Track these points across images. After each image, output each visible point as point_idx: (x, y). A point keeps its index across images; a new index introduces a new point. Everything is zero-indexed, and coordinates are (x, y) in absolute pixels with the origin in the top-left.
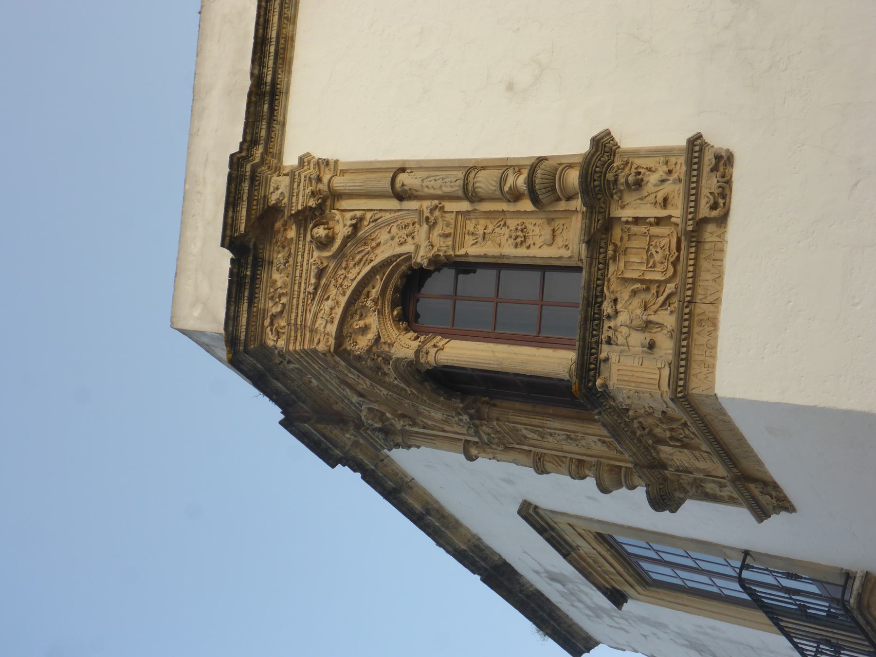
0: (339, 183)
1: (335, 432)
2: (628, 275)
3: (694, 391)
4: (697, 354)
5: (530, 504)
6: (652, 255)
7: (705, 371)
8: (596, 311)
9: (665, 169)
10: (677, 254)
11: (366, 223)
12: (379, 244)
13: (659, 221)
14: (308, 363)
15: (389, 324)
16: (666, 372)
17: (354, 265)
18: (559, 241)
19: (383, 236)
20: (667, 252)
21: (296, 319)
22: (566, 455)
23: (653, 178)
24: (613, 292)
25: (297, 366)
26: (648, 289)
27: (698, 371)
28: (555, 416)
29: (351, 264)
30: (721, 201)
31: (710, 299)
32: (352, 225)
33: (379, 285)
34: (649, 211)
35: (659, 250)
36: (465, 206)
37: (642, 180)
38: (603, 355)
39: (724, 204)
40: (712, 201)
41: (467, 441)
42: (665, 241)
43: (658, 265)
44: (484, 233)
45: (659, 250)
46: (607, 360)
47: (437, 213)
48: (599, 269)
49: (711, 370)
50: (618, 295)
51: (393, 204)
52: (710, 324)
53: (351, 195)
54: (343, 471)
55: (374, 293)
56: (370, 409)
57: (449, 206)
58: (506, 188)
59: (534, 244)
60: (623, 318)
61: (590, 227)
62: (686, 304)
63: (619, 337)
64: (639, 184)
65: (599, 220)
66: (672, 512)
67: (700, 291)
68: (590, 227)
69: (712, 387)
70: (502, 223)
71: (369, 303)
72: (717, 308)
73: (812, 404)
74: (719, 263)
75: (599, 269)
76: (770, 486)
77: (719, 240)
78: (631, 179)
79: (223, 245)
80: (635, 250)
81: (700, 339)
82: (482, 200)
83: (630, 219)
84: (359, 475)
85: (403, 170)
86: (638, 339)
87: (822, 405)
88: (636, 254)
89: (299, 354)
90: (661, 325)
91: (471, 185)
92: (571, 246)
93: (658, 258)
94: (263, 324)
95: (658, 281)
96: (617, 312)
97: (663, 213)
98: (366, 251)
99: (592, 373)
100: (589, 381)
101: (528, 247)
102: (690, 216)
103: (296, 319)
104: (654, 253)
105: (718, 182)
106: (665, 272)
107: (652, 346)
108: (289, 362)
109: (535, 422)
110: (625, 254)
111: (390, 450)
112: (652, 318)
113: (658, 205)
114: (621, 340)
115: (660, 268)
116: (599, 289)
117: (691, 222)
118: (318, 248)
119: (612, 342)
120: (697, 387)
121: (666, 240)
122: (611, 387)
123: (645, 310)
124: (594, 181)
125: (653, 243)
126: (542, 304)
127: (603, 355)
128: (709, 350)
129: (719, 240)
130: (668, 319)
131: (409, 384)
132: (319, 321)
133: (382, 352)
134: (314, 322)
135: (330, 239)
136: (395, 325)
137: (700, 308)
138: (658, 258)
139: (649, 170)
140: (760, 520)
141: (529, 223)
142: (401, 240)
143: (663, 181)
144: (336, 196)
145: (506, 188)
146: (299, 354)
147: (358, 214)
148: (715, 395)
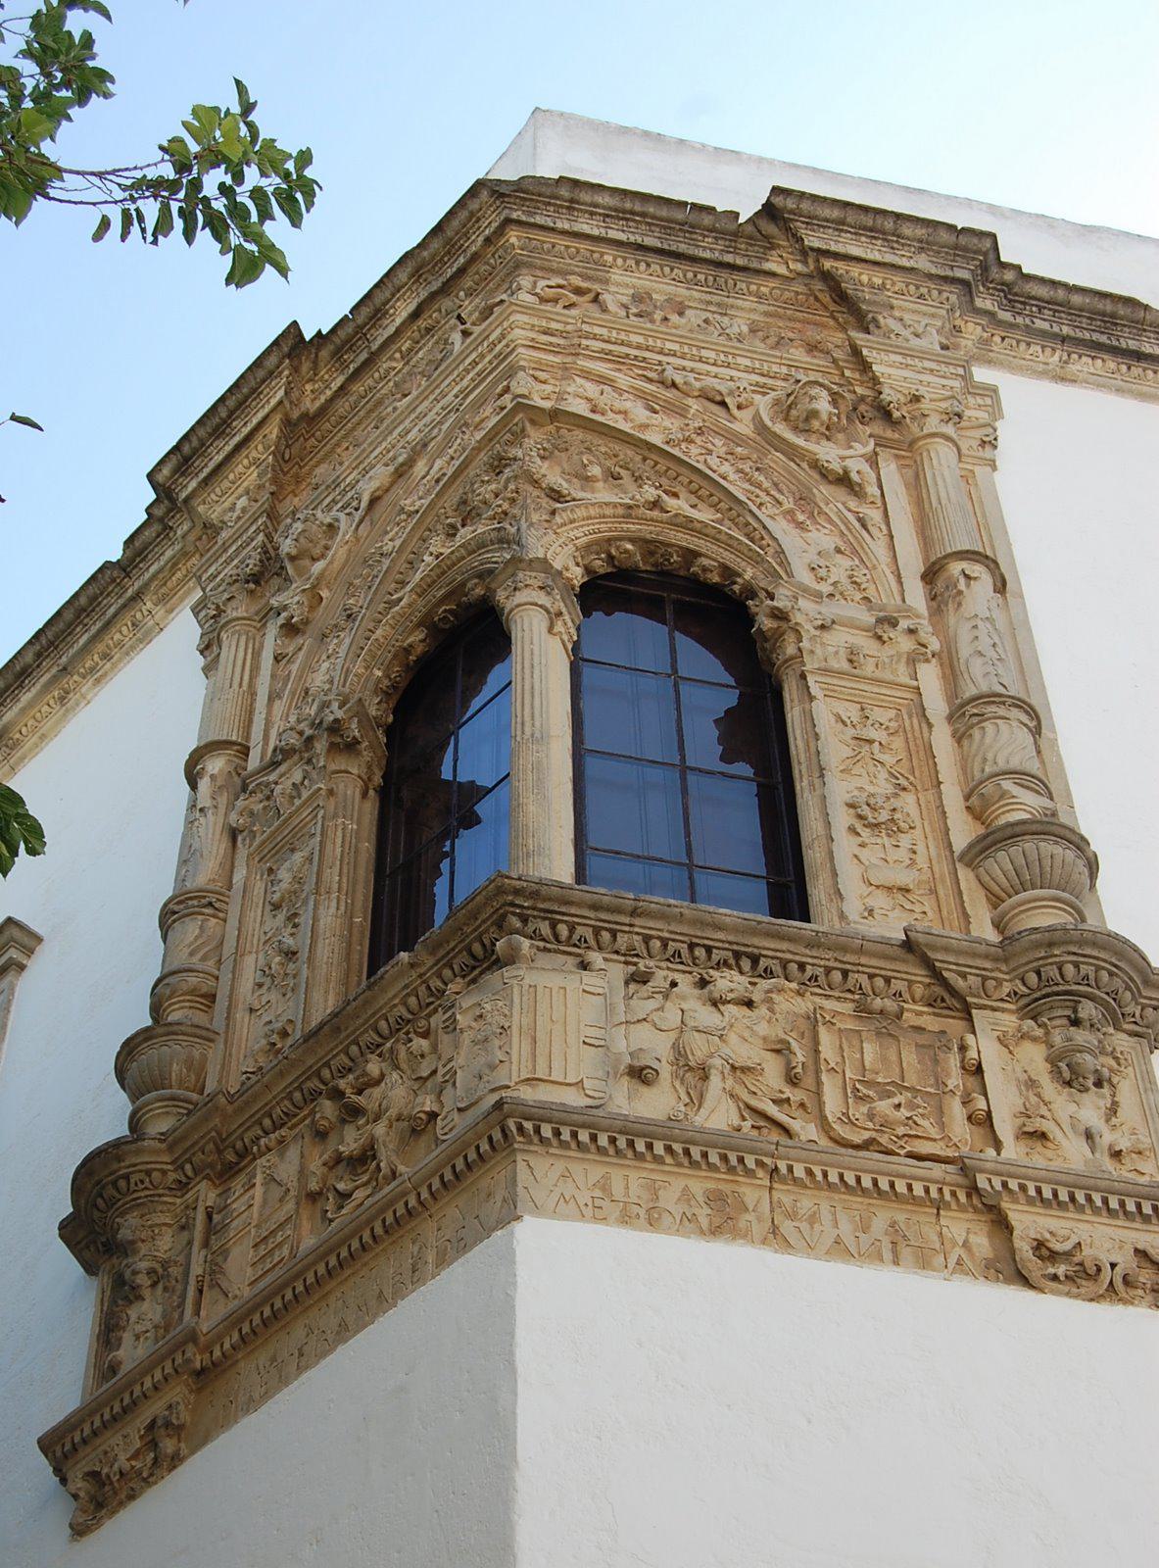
0: (941, 460)
1: (248, 475)
2: (826, 1038)
3: (521, 1166)
4: (629, 1180)
5: (30, 952)
6: (890, 1095)
7: (584, 1197)
8: (716, 955)
9: (1123, 1144)
10: (902, 1152)
11: (853, 504)
12: (800, 525)
13: (984, 1122)
14: (475, 363)
15: (605, 529)
16: (573, 1099)
17: (741, 471)
18: (880, 901)
19: (823, 538)
20: (901, 1131)
21: (595, 337)
22: (227, 966)
23: (1090, 1110)
24: (770, 1000)
25: (457, 347)
26: (792, 1080)
27: (580, 1179)
28: (366, 900)
29: (746, 467)
30: (1061, 1270)
31: (787, 1227)
32: (846, 472)
33: (704, 515)
34: (1004, 1102)
35: (904, 1112)
36: (936, 704)
37: (1084, 1090)
38: (596, 958)
39: (1055, 1278)
40: (1058, 1247)
41: (245, 751)
42: (928, 1126)
43: (864, 1109)
44: (870, 742)
45: (904, 1112)
46: (584, 966)
47: (906, 644)
48: (828, 971)
49: (588, 1212)
50: (763, 1011)
51: (913, 563)
52: (717, 1221)
53: (917, 486)
54: (135, 502)
55: (680, 505)
56: (332, 529)
57: (930, 677)
58: (1007, 785)
59: (862, 845)
60: (707, 1016)
61: (946, 949)
62: (767, 1160)
63: (652, 1004)
64: (1071, 1078)
65: (964, 976)
66: (63, 1226)
67: (806, 1203)
68: (946, 949)
69: (537, 1209)
70: (903, 782)
71: (650, 492)
72: (764, 1241)
73: (522, 1453)
74: (887, 1255)
75: (828, 971)
76: (163, 1450)
77: (951, 1265)
78: (1088, 1061)
79: (776, 190)
80: (894, 1058)
81: (680, 1186)
82: (959, 738)
83: (972, 1054)
84: (116, 554)
85: (1001, 586)
86: (656, 1047)
87: (520, 1482)
88: (884, 1059)
89: (503, 336)
90: (697, 1100)
91: (1002, 711)
92: (870, 921)
93: (884, 1106)
94: (573, 273)
95: (821, 1104)
96: (716, 1003)
97: (1005, 1128)
98: (781, 498)
99: (545, 928)
100: (525, 920)
101: (852, 830)
102: (1013, 1185)
103: (595, 337)
104: (896, 1101)
105: (1113, 1266)
106: (847, 1119)
107: (641, 1075)
108: (466, 334)
109: (332, 876)
110: (878, 1034)
111: (196, 610)
112: (715, 1080)
113: (1019, 1121)
114: (644, 1007)
115: (859, 1112)
116: (777, 969)
117: (997, 1183)
118: (777, 402)
119: (633, 987)
120: (538, 1171)
121: (934, 1133)
122: (507, 972)
123: (733, 1068)
124: (1076, 965)
125: (919, 1101)
126: (690, 867)
127: (596, 958)
128: (642, 1213)
129: (951, 1265)
130: (718, 1115)
131: (422, 591)
132: (592, 390)
133: (524, 507)
134: (586, 375)
135: (804, 424)
136: (597, 542)
137: (753, 1193)
138: (884, 1106)
139: (1113, 1110)
140: (46, 1444)
141: (920, 840)
142: (820, 575)
143: (1089, 1136)
144: (910, 452)
145: (1007, 785)
146: (503, 336)
147: (872, 490)
148: (519, 1218)
